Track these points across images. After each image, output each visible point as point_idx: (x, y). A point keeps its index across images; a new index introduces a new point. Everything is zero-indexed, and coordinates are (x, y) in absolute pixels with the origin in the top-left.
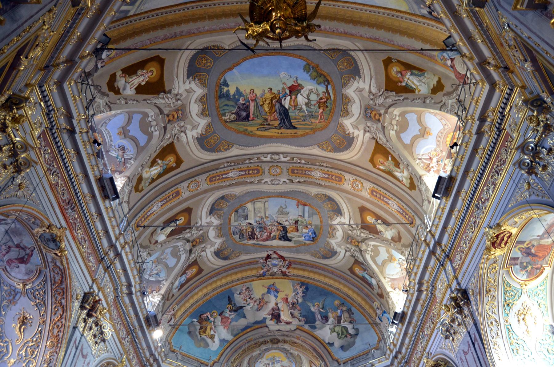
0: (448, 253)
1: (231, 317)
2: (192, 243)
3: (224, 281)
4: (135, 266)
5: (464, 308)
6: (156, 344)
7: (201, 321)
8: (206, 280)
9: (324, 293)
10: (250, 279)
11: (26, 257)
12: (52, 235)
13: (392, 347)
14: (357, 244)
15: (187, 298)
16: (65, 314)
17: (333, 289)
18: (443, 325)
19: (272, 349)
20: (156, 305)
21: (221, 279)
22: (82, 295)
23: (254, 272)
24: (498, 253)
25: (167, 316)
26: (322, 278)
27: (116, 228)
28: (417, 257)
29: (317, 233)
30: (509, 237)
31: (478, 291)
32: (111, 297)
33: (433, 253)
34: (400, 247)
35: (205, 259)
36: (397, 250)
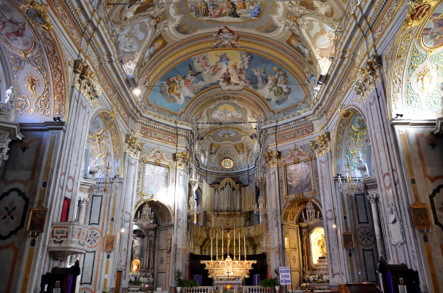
0: (372, 25)
1: (192, 80)
2: (156, 19)
3: (185, 52)
4: (111, 39)
5: (377, 70)
6: (137, 100)
7: (169, 83)
8: (171, 51)
9: (266, 61)
10: (206, 50)
11: (20, 31)
12: (36, 11)
13: (315, 101)
14: (295, 19)
15: (156, 66)
16: (63, 77)
17: (273, 58)
18: (357, 84)
19: (224, 103)
20: (133, 71)
21: (182, 50)
22: (73, 62)
23: (209, 45)
24: (415, 24)
25: (142, 80)
26: (264, 49)
27: (90, 5)
28: (345, 29)
29: (262, 10)
30: (428, 10)
31: (390, 56)
32: (97, 64)
33: (359, 25)
34: (331, 22)
35: (168, 34)
36: (328, 24)
